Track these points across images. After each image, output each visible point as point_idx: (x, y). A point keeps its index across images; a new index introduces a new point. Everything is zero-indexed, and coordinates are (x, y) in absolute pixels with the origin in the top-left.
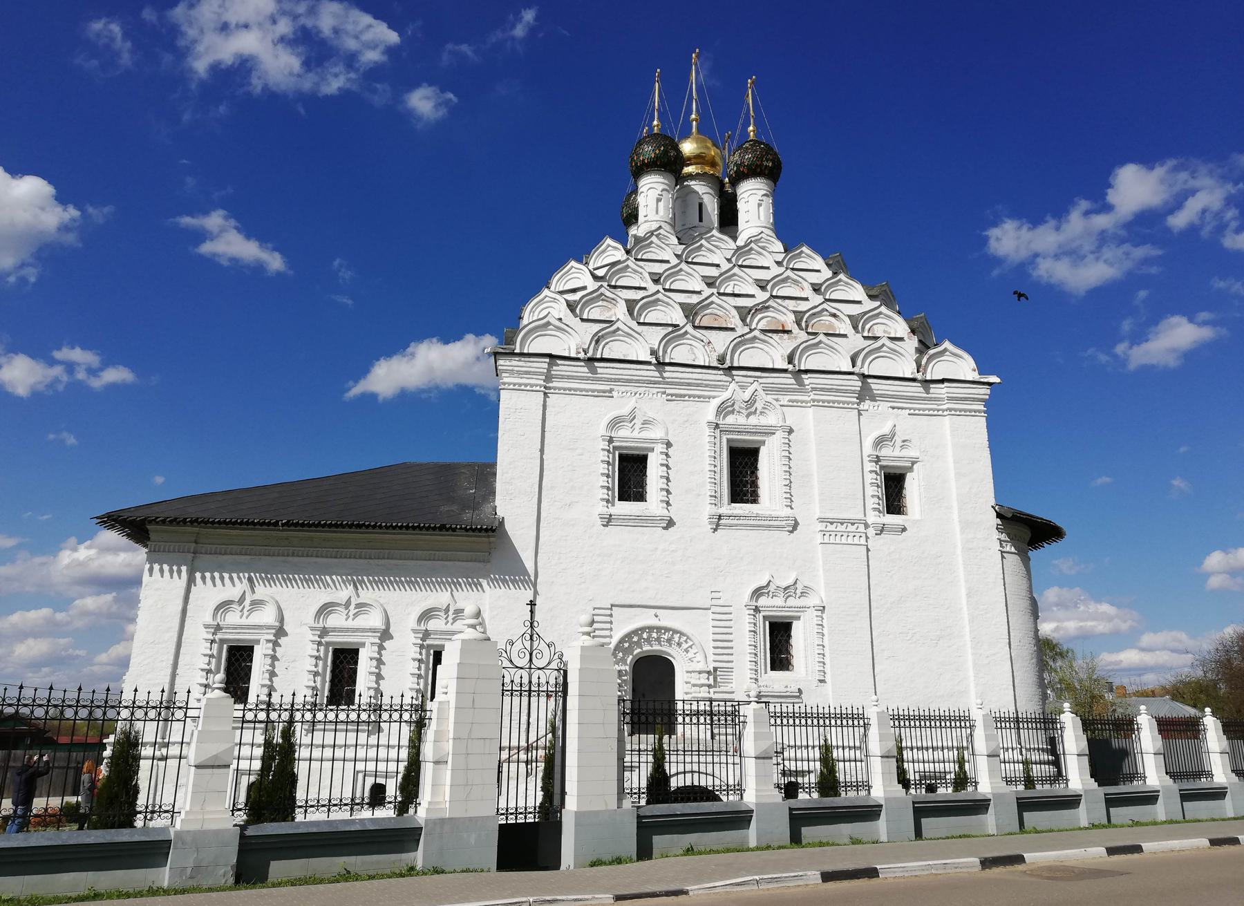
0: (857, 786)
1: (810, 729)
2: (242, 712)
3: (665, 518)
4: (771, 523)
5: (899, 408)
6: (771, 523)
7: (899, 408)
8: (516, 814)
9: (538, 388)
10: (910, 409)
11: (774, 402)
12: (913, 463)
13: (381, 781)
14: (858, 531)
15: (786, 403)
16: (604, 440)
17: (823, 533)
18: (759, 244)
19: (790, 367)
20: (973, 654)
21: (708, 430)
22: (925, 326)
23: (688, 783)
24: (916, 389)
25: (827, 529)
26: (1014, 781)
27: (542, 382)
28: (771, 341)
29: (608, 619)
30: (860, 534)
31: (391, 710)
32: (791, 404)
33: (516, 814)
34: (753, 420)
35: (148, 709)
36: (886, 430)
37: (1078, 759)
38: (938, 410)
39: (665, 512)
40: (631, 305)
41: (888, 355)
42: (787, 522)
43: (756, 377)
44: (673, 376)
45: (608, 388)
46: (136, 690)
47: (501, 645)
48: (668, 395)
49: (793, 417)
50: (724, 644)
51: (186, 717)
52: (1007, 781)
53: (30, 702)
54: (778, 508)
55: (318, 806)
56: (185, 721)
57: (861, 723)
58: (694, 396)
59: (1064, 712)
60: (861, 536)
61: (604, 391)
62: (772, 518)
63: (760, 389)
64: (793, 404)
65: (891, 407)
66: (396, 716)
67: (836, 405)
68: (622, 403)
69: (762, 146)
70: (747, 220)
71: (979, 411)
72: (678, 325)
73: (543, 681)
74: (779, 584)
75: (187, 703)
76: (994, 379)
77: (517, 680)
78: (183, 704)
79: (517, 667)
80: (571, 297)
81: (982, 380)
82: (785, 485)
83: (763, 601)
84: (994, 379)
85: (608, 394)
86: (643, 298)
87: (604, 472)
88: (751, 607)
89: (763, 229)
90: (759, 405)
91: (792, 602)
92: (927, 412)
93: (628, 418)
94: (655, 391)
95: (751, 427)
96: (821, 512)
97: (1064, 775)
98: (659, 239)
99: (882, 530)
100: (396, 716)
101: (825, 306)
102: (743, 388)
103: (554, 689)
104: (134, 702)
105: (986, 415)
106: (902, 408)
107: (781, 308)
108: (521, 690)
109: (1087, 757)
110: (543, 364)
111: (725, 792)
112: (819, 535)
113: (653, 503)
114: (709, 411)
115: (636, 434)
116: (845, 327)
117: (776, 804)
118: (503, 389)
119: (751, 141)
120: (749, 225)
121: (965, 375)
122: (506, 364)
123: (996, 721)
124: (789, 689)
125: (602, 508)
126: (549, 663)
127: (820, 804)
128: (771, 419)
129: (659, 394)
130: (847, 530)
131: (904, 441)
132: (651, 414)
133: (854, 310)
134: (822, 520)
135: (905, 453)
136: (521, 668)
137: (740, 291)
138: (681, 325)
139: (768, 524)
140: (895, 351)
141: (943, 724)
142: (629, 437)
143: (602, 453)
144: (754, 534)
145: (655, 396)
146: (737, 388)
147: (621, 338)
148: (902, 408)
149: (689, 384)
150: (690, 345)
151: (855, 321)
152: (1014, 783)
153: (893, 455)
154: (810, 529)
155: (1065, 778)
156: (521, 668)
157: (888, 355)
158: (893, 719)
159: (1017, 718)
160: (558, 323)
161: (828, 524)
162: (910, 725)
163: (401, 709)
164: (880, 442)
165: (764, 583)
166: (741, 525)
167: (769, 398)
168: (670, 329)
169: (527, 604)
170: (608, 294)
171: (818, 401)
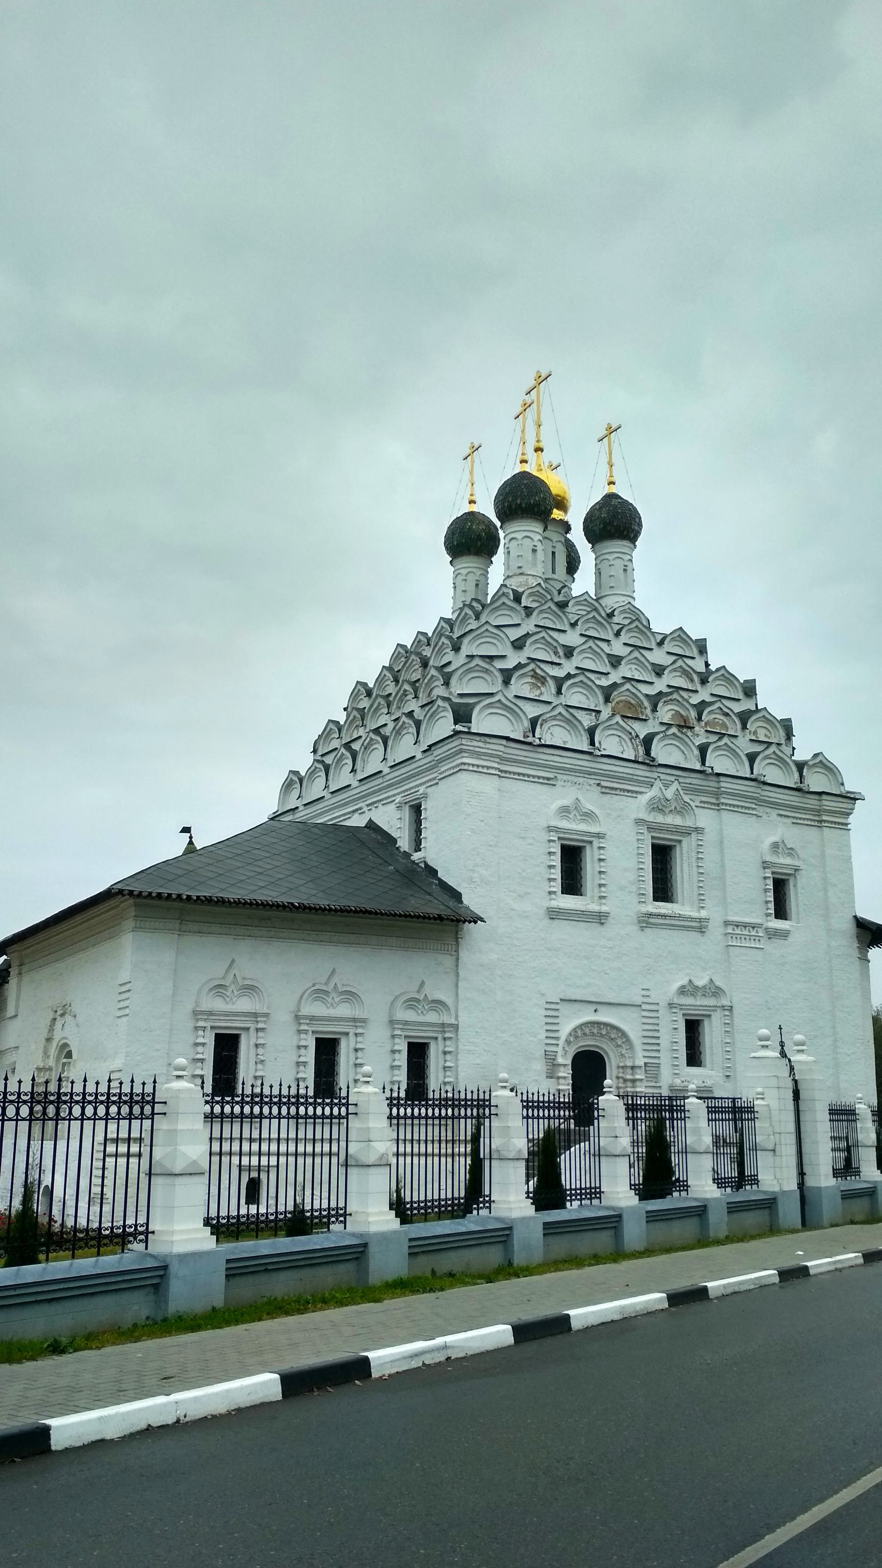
1: (284, 1122)
10: (794, 817)
13: (254, 1174)
32: (703, 805)
34: (677, 820)
43: (677, 776)
48: (603, 787)
50: (652, 1041)
58: (624, 790)
61: (548, 779)
85: (549, 782)
94: (592, 782)
97: (487, 1193)
102: (667, 786)
106: (788, 817)
109: (250, 1206)
122: (468, 744)
124: (706, 1084)
127: (233, 1253)
144: (674, 933)
148: (788, 817)
154: (716, 931)
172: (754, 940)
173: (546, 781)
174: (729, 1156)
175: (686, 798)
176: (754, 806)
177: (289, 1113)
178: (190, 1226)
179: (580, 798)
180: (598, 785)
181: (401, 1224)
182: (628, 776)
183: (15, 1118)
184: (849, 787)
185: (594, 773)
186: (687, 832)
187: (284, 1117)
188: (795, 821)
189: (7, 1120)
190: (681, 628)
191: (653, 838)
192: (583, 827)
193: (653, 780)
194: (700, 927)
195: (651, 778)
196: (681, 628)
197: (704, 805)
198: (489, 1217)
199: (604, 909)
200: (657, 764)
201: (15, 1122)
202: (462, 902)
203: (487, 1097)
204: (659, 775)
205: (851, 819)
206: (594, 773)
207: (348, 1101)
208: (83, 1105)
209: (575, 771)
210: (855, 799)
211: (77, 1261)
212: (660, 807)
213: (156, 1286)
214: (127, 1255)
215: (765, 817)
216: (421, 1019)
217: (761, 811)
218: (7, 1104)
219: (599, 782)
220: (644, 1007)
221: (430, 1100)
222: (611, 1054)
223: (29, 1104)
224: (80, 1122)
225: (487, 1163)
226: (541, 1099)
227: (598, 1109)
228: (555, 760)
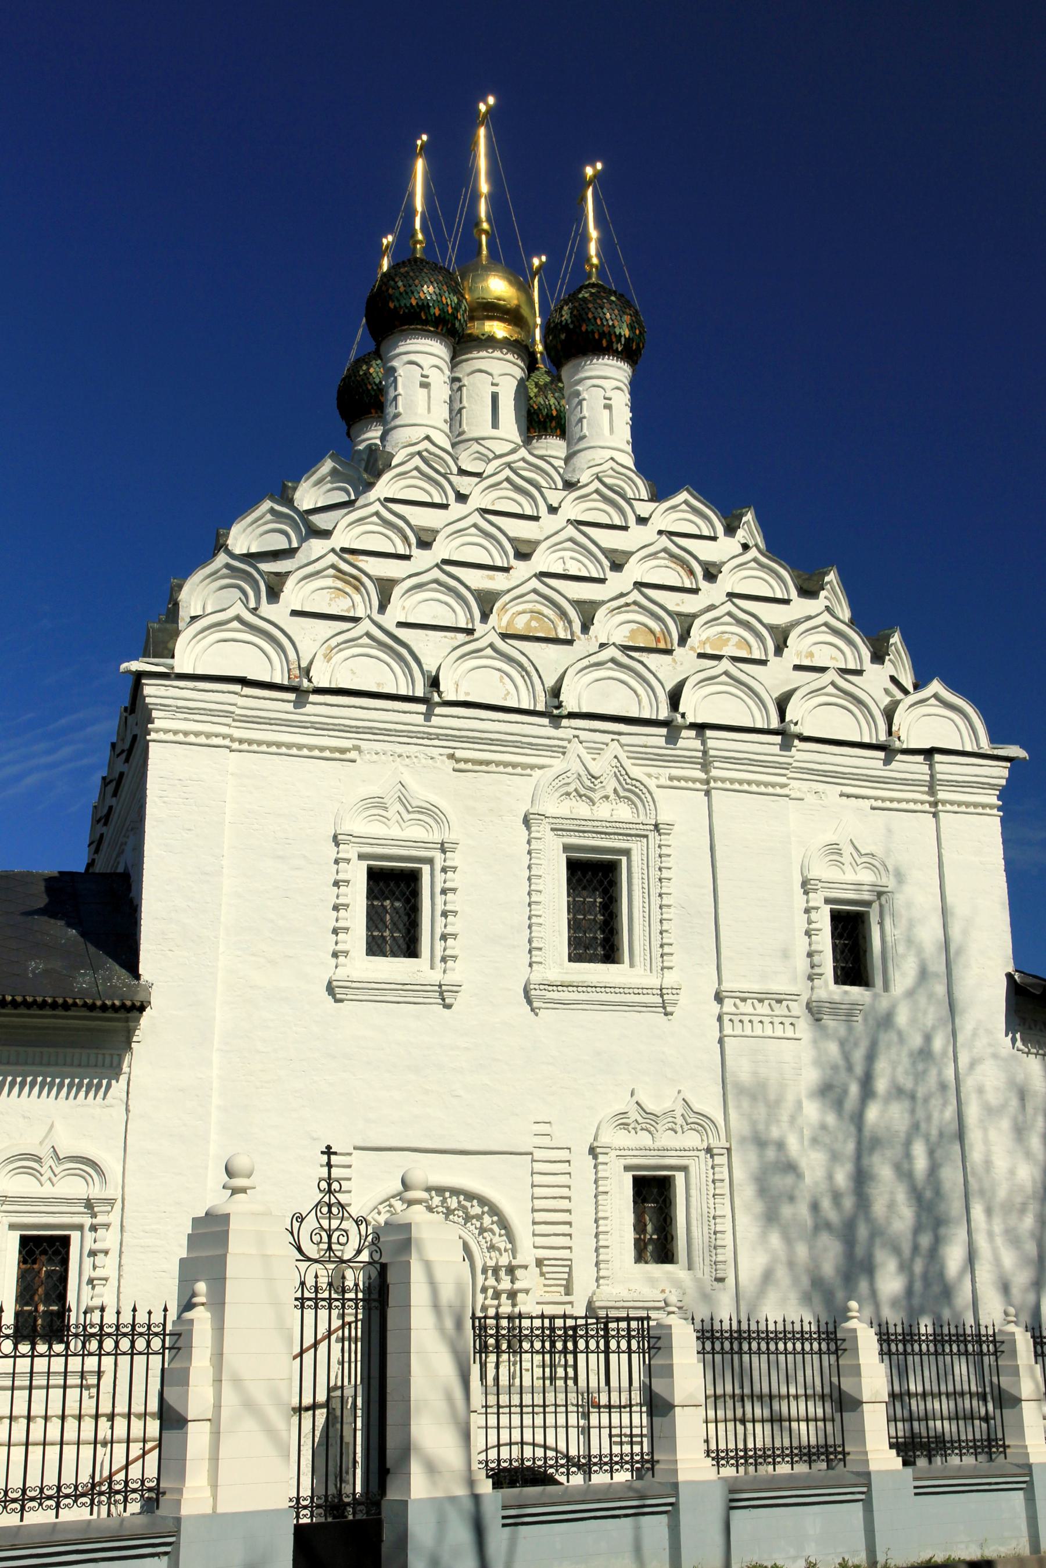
0: (611, 1463)
5: (857, 797)
7: (857, 797)
10: (876, 799)
26: (769, 1456)
29: (538, 1179)
48: (458, 761)
52: (717, 1459)
55: (41, 1498)
57: (833, 1347)
58: (506, 764)
66: (125, 1344)
69: (613, 298)
71: (991, 807)
76: (1015, 751)
79: (309, 1259)
81: (996, 752)
84: (1015, 751)
86: (410, 576)
97: (1000, 1436)
100: (125, 1344)
105: (1001, 814)
106: (863, 798)
108: (343, 1299)
111: (563, 1470)
115: (395, 832)
117: (897, 1471)
118: (154, 741)
119: (593, 285)
125: (326, 969)
136: (316, 1261)
141: (772, 1347)
148: (863, 798)
149: (492, 742)
152: (606, 1467)
155: (1001, 1443)
159: (979, 1335)
161: (738, 1001)
162: (768, 1349)
168: (462, 637)
169: (323, 1153)
173: (337, 755)
174: (605, 1432)
175: (636, 772)
176: (783, 780)
177: (812, 1349)
179: (408, 780)
180: (451, 756)
183: (30, 1354)
187: (592, 1352)
189: (136, 1354)
191: (566, 848)
192: (417, 832)
197: (675, 783)
199: (450, 978)
200: (565, 712)
201: (97, 1358)
202: (137, 977)
204: (577, 732)
207: (836, 1336)
208: (133, 1338)
209: (398, 733)
212: (583, 791)
215: (810, 798)
216: (47, 1190)
217: (797, 787)
218: (136, 1337)
219: (451, 751)
220: (539, 1154)
221: (915, 1335)
223: (130, 1337)
224: (30, 1359)
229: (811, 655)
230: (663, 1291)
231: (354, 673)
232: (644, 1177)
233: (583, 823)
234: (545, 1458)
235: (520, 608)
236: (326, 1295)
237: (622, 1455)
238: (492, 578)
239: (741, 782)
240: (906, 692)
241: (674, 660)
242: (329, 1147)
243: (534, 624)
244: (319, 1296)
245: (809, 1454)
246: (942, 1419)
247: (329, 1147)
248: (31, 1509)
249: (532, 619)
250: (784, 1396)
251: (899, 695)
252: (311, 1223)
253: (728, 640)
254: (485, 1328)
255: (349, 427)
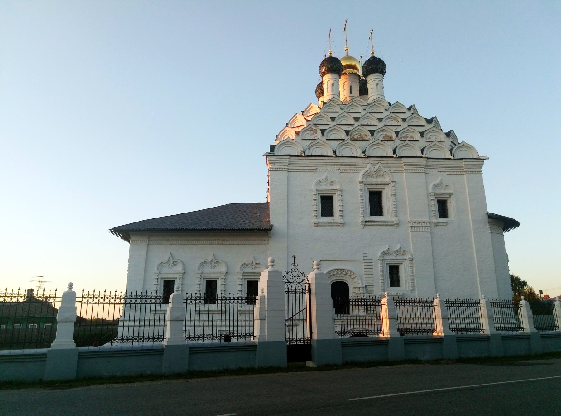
2: (81, 298)
3: (342, 223)
4: (388, 224)
5: (443, 172)
6: (388, 224)
8: (297, 340)
9: (285, 170)
10: (448, 172)
11: (388, 171)
12: (450, 195)
14: (427, 226)
15: (393, 171)
16: (314, 191)
17: (412, 227)
18: (378, 102)
19: (395, 156)
20: (479, 278)
21: (359, 185)
22: (454, 136)
23: (405, 327)
24: (424, 161)
25: (413, 226)
26: (478, 330)
27: (287, 167)
28: (385, 144)
30: (427, 227)
31: (230, 300)
32: (395, 171)
33: (297, 340)
34: (379, 180)
35: (12, 298)
36: (438, 181)
37: (528, 320)
38: (461, 172)
39: (342, 221)
40: (323, 132)
41: (438, 149)
42: (395, 223)
44: (343, 162)
45: (315, 168)
46: (105, 291)
47: (283, 274)
49: (397, 177)
51: (55, 301)
52: (497, 330)
53: (119, 297)
54: (391, 217)
55: (208, 337)
56: (54, 303)
59: (556, 301)
60: (428, 228)
61: (313, 170)
62: (388, 222)
63: (381, 166)
64: (396, 171)
65: (439, 171)
67: (415, 171)
68: (322, 175)
70: (372, 92)
72: (344, 140)
73: (294, 288)
74: (393, 250)
75: (55, 295)
77: (297, 288)
78: (54, 296)
79: (290, 282)
80: (297, 130)
82: (394, 207)
83: (386, 257)
85: (314, 171)
86: (328, 128)
87: (340, 204)
88: (381, 260)
89: (379, 96)
90: (382, 173)
91: (399, 257)
92: (455, 173)
93: (324, 181)
95: (378, 182)
96: (410, 218)
97: (522, 326)
98: (334, 102)
99: (438, 225)
101: (408, 128)
102: (374, 166)
103: (291, 291)
104: (5, 294)
107: (388, 130)
110: (287, 159)
112: (410, 228)
113: (337, 217)
114: (359, 176)
115: (328, 188)
116: (418, 137)
120: (373, 94)
121: (387, 154)
122: (271, 160)
123: (491, 304)
125: (314, 220)
126: (303, 281)
128: (387, 179)
129: (337, 170)
130: (422, 226)
131: (446, 186)
132: (334, 179)
133: (422, 129)
134: (411, 221)
135: (447, 191)
136: (292, 283)
137: (370, 123)
138: (345, 140)
139: (388, 224)
140: (440, 146)
141: (495, 306)
142: (326, 189)
143: (314, 196)
145: (335, 171)
146: (371, 166)
147: (320, 146)
148: (445, 172)
150: (350, 148)
151: (422, 134)
153: (442, 192)
156: (292, 283)
157: (438, 149)
158: (447, 303)
160: (292, 141)
161: (413, 223)
163: (115, 298)
164: (436, 186)
165: (386, 249)
166: (375, 225)
167: (386, 170)
168: (341, 141)
169: (293, 257)
170: (313, 128)
171: (407, 170)
172: (420, 228)
178: (395, 331)
181: (76, 346)
182: (353, 164)
184: (481, 154)
185: (335, 165)
186: (387, 184)
188: (449, 173)
190: (397, 102)
191: (368, 189)
193: (367, 164)
194: (397, 224)
195: (366, 163)
196: (397, 102)
198: (383, 337)
203: (478, 301)
205: (483, 169)
206: (335, 165)
210: (484, 159)
211: (550, 332)
213: (529, 338)
214: (553, 332)
219: (339, 168)
222: (346, 279)
225: (521, 319)
226: (510, 302)
227: (555, 305)
228: (348, 168)
229: (430, 138)
230: (397, 293)
231: (316, 152)
232: (392, 266)
233: (372, 182)
234: (360, 331)
235: (355, 133)
236: (301, 291)
237: (372, 330)
238: (349, 127)
239: (412, 170)
240: (455, 145)
241: (394, 142)
242: (294, 256)
243: (359, 137)
244: (293, 291)
245: (516, 329)
246: (465, 324)
247: (294, 256)
248: (240, 338)
249: (359, 136)
250: (429, 318)
251: (454, 146)
252: (290, 273)
253: (408, 136)
254: (355, 301)
255: (318, 99)
